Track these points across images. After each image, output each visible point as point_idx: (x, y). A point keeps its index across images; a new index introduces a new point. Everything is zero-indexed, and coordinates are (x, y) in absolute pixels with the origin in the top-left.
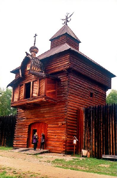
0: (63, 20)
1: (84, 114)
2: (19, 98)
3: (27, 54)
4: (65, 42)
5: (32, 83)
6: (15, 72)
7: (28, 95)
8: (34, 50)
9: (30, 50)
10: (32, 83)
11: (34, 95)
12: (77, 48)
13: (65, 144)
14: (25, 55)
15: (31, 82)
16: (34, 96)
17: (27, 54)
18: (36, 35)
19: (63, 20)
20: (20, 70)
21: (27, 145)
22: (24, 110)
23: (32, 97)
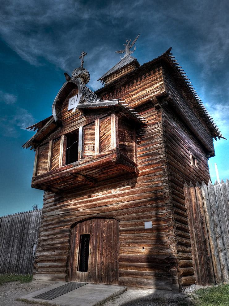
5: (81, 129)
10: (81, 129)
15: (77, 130)
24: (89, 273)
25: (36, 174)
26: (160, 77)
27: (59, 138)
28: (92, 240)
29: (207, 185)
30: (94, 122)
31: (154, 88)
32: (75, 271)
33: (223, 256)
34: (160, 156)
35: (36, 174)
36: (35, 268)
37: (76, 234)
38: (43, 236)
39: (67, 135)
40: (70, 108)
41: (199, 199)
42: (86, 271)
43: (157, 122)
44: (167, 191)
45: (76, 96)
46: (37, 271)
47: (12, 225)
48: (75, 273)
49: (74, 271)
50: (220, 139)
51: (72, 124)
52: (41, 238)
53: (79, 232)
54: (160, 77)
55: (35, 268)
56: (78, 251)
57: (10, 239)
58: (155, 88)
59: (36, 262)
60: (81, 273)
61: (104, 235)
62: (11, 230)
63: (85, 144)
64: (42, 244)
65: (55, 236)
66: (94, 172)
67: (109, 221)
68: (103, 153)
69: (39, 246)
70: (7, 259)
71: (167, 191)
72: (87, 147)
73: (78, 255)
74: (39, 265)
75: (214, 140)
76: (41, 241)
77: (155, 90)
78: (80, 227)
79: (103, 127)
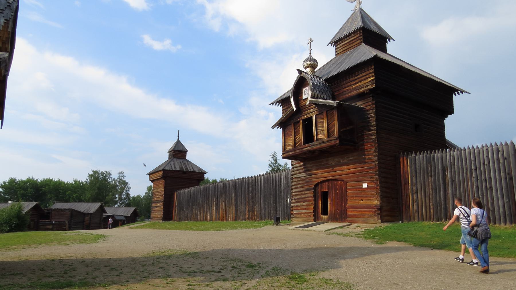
0: (126, 176)
1: (490, 208)
2: (295, 144)
3: (300, 72)
4: (361, 42)
5: (314, 118)
6: (284, 102)
7: (309, 137)
8: (313, 64)
9: (317, 61)
10: (314, 118)
11: (320, 137)
12: (384, 50)
13: (379, 212)
14: (297, 74)
15: (312, 117)
16: (321, 139)
17: (300, 72)
18: (311, 41)
19: (126, 176)
20: (292, 100)
21: (314, 216)
22: (303, 162)
23: (317, 139)
24: (329, 216)
25: (285, 149)
26: (372, 73)
27: (299, 122)
28: (330, 195)
29: (412, 155)
30: (323, 113)
31: (368, 81)
32: (320, 215)
33: (416, 205)
34: (373, 136)
35: (285, 149)
36: (292, 214)
37: (318, 191)
38: (295, 192)
39: (304, 121)
40: (304, 97)
41: (405, 167)
42: (327, 215)
43: (372, 108)
44: (377, 163)
45: (308, 87)
46: (294, 215)
47: (265, 183)
48: (320, 216)
49: (319, 215)
50: (463, 94)
51: (307, 112)
52: (293, 193)
53: (321, 190)
54: (372, 73)
55: (292, 214)
56: (321, 203)
57: (266, 194)
58: (369, 82)
59: (292, 210)
60: (324, 216)
61: (338, 192)
62: (265, 186)
63: (318, 129)
64: (295, 198)
65: (304, 193)
66: (306, 213)
67: (341, 183)
68: (330, 139)
69: (292, 199)
70: (56, 281)
71: (377, 163)
72: (319, 132)
73: (321, 205)
74: (295, 212)
75: (454, 96)
76: (293, 196)
77: (368, 84)
78: (321, 186)
79: (329, 118)
